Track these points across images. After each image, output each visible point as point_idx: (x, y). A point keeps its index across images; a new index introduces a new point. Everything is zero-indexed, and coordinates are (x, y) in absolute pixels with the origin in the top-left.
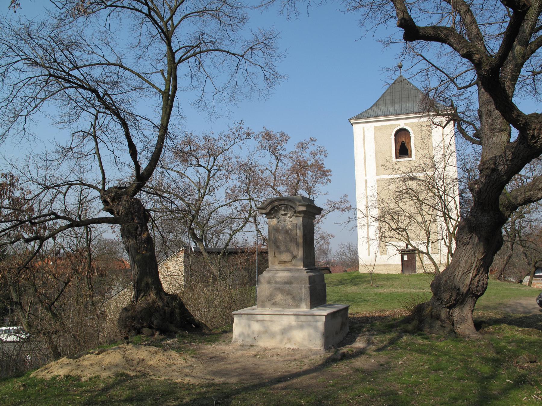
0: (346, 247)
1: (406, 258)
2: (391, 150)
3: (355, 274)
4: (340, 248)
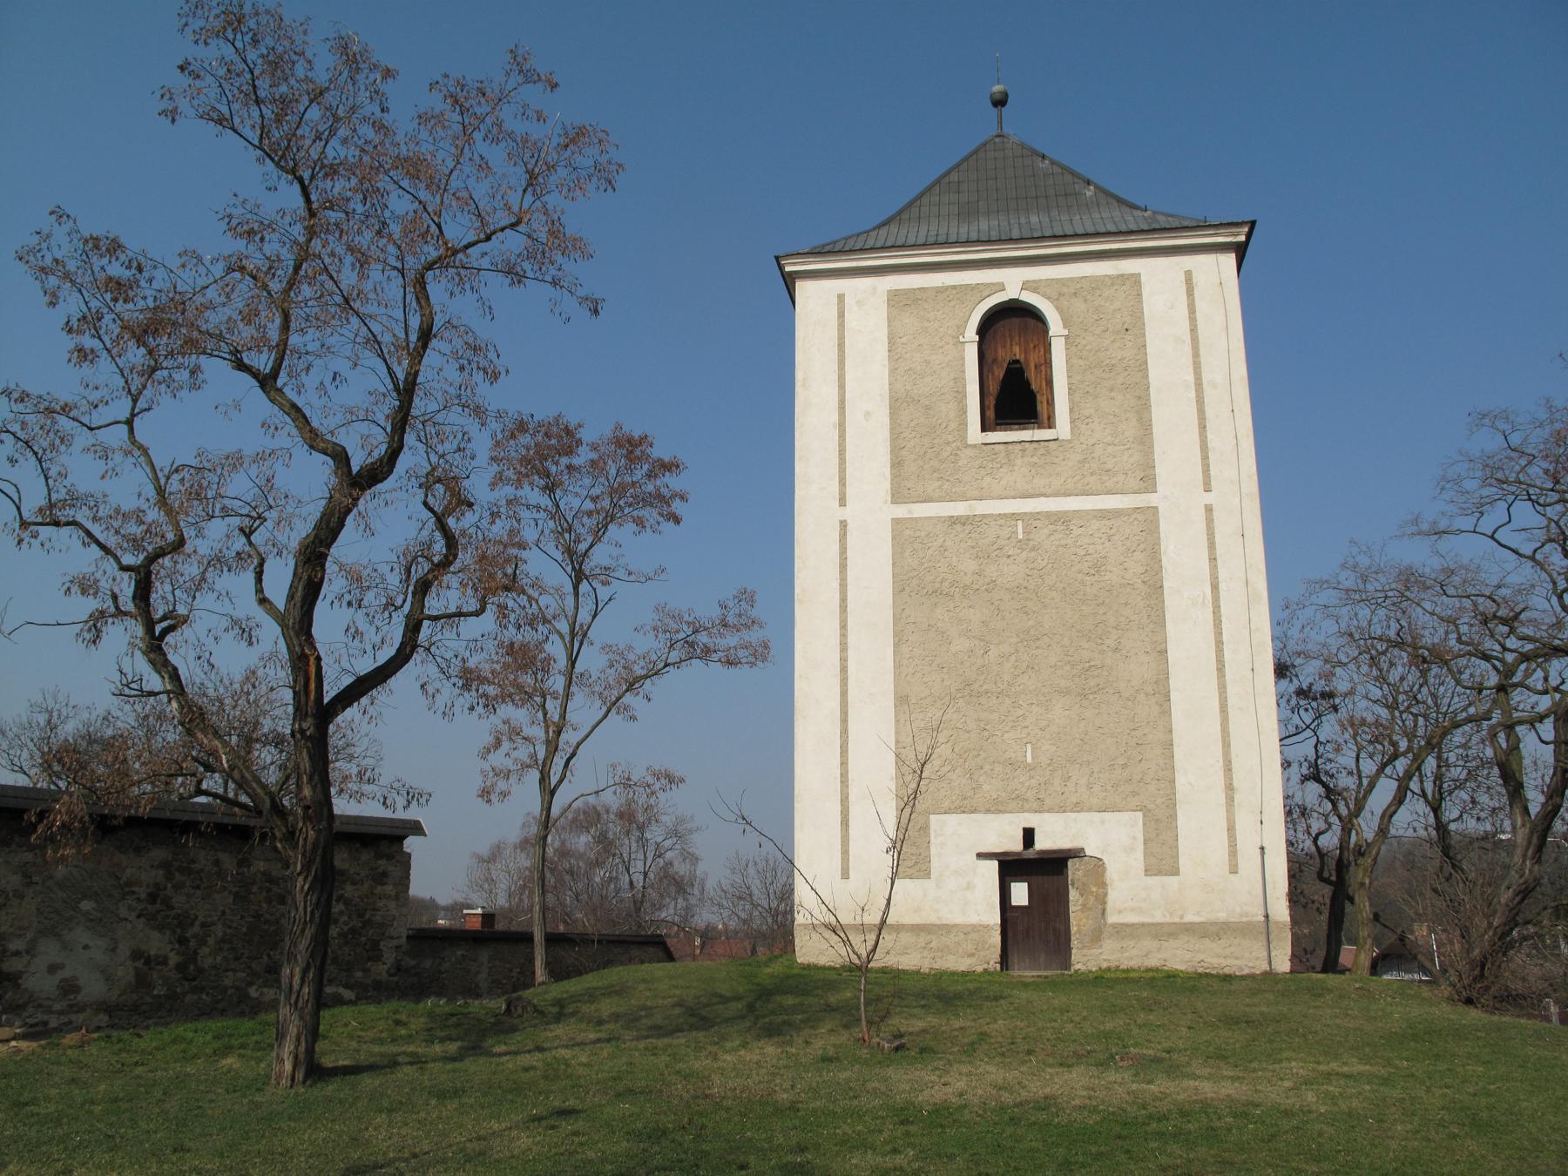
0: (751, 871)
1: (1020, 894)
2: (961, 395)
3: (777, 968)
4: (733, 871)
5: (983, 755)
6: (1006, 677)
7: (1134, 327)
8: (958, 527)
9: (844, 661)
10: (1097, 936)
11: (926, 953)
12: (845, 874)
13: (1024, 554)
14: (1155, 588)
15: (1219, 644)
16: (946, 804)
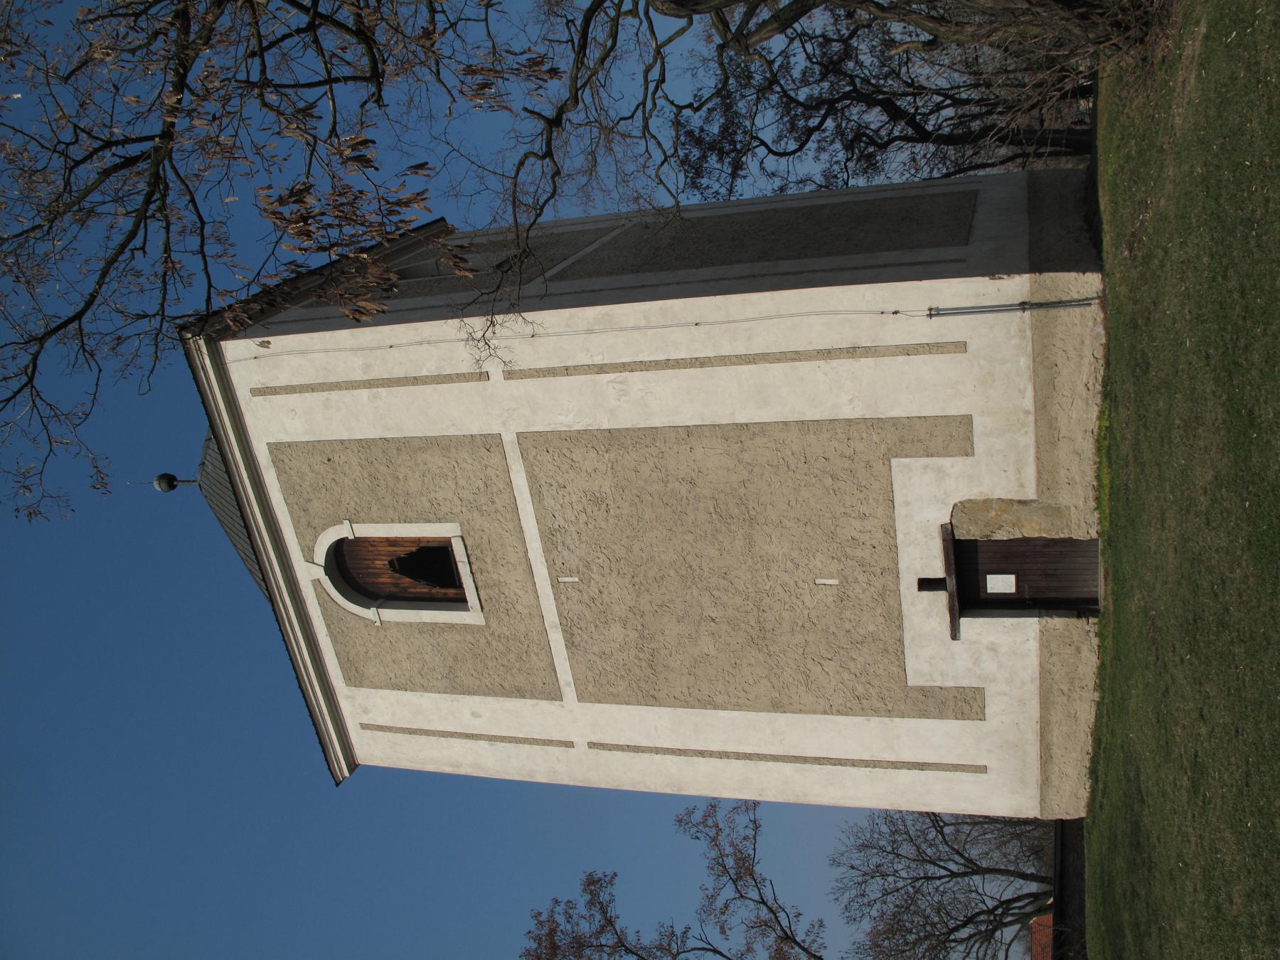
1: (1000, 584)
5: (833, 629)
6: (738, 601)
7: (327, 452)
8: (577, 640)
9: (738, 756)
10: (1056, 512)
11: (1075, 696)
12: (983, 769)
13: (595, 576)
14: (613, 438)
15: (668, 364)
16: (894, 669)
